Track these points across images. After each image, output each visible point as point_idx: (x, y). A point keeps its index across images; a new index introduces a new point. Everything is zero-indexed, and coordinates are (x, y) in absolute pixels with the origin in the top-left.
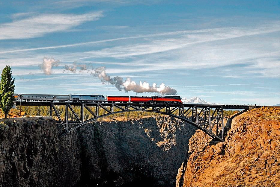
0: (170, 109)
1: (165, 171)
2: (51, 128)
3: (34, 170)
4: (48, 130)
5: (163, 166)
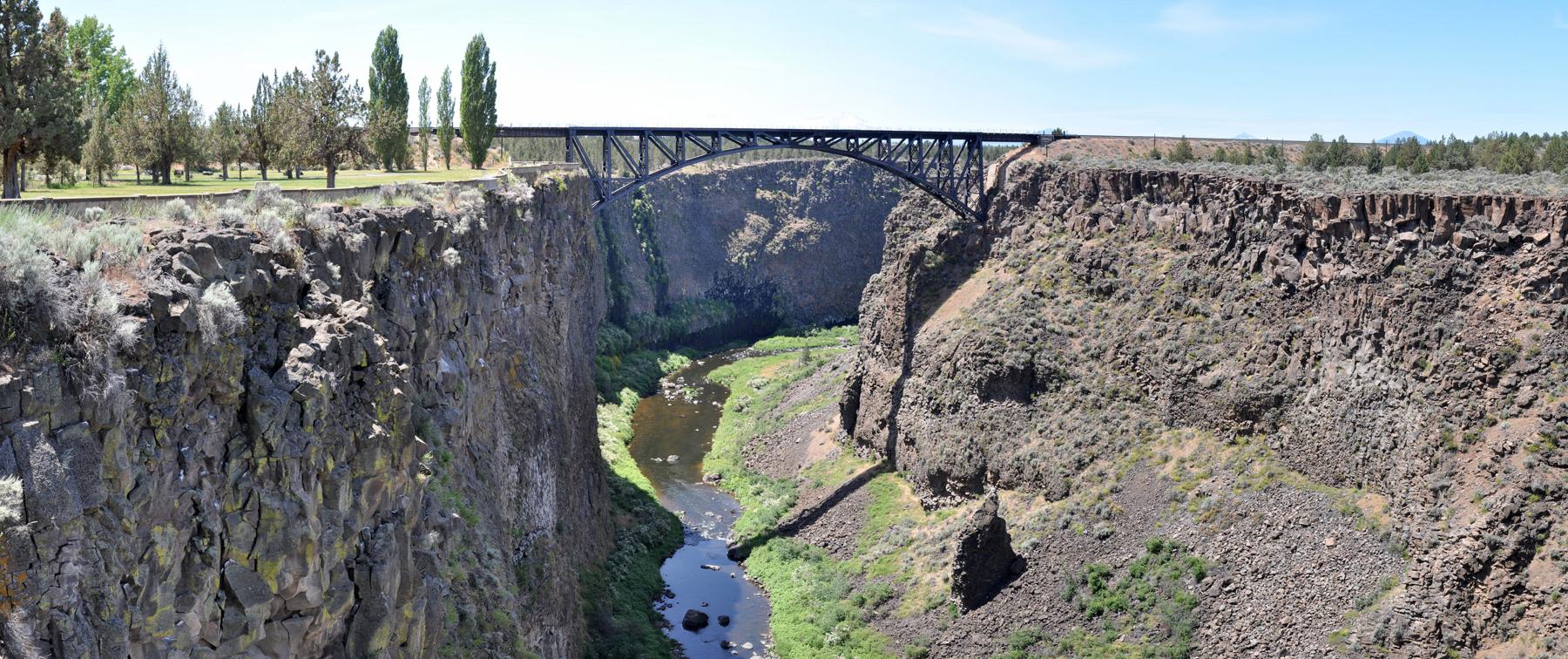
2: (578, 194)
3: (562, 292)
4: (572, 196)
5: (800, 283)
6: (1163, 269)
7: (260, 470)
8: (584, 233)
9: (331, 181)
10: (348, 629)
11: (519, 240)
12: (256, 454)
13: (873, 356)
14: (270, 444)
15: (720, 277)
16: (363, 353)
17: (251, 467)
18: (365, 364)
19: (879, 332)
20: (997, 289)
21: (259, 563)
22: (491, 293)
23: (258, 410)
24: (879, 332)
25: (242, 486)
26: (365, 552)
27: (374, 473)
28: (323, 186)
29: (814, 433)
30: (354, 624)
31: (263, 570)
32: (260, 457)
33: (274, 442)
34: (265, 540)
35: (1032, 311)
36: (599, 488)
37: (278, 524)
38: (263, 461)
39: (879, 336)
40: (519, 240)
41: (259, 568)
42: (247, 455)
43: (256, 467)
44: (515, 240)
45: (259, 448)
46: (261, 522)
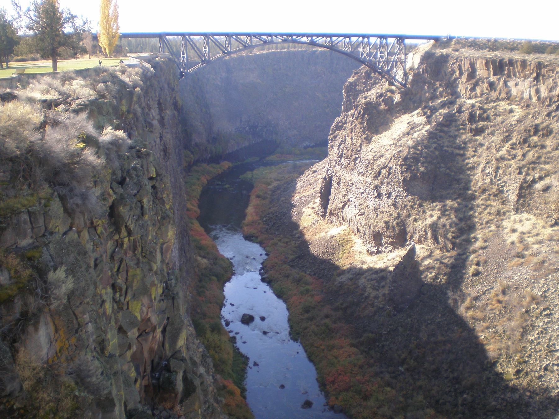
0: (331, 39)
1: (293, 131)
6: (515, 118)
7: (125, 246)
8: (174, 96)
9: (55, 67)
10: (164, 337)
11: (151, 100)
12: (122, 236)
13: (339, 165)
14: (130, 229)
15: (243, 120)
16: (153, 169)
17: (119, 244)
18: (155, 176)
19: (342, 151)
20: (413, 127)
21: (130, 303)
22: (152, 132)
23: (121, 208)
24: (342, 151)
25: (116, 258)
26: (166, 288)
27: (166, 241)
28: (51, 70)
29: (304, 209)
30: (167, 333)
31: (132, 307)
32: (124, 238)
33: (132, 227)
34: (132, 290)
35: (435, 140)
36: (189, 244)
37: (139, 278)
38: (126, 240)
39: (342, 154)
40: (151, 100)
41: (130, 307)
42: (116, 237)
43: (122, 244)
44: (149, 100)
45: (124, 233)
46: (129, 278)
